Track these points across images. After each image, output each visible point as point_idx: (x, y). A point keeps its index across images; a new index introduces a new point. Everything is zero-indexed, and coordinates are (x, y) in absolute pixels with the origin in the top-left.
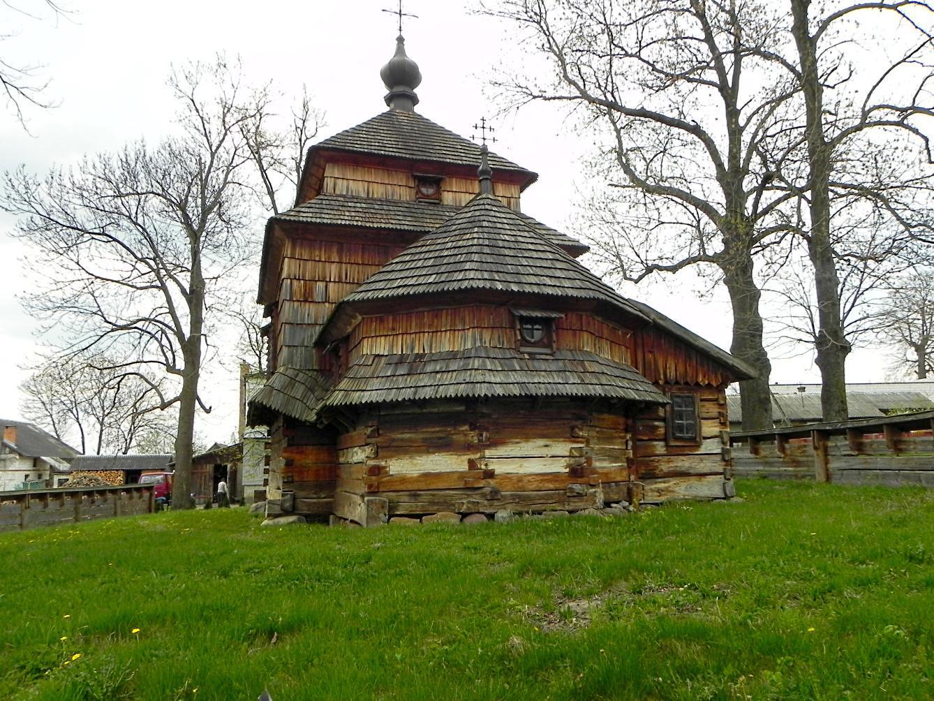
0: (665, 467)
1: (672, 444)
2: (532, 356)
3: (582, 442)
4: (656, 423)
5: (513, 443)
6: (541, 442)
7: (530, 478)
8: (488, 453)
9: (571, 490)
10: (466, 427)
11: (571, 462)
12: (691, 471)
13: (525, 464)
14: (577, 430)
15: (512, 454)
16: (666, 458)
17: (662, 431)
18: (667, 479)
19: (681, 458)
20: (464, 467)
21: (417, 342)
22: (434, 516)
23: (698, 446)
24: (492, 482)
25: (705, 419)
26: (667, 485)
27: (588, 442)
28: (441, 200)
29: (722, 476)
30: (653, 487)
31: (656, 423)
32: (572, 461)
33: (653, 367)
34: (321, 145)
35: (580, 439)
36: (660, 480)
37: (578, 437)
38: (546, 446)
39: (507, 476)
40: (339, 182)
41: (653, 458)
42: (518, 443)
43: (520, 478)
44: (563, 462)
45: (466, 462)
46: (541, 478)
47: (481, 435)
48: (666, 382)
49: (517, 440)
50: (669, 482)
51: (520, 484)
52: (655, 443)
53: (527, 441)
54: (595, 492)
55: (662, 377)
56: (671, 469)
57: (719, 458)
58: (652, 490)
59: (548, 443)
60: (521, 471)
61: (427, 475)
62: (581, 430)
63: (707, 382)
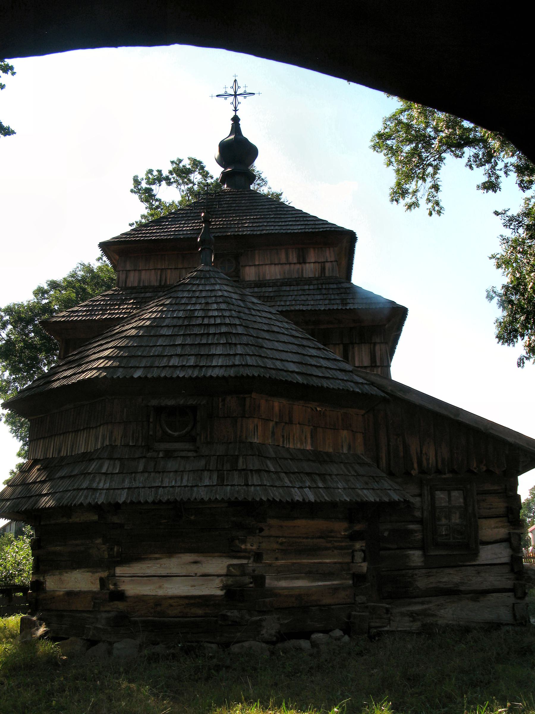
0: (422, 583)
1: (433, 553)
2: (169, 455)
3: (248, 558)
4: (412, 527)
5: (151, 559)
6: (188, 557)
7: (171, 601)
8: (119, 571)
9: (224, 617)
10: (99, 541)
11: (230, 582)
12: (462, 588)
13: (166, 585)
14: (237, 542)
15: (150, 572)
16: (424, 571)
17: (419, 536)
18: (427, 599)
19: (447, 570)
20: (96, 587)
21: (64, 444)
22: (67, 641)
23: (475, 554)
24: (121, 606)
25: (485, 518)
26: (425, 606)
27: (258, 557)
28: (239, 277)
29: (510, 594)
30: (404, 609)
31: (412, 527)
32: (230, 581)
33: (402, 454)
34: (114, 240)
35: (242, 554)
36: (417, 600)
37: (239, 552)
38: (196, 562)
39: (141, 599)
40: (132, 274)
41: (404, 572)
42: (157, 559)
43: (158, 601)
44: (217, 582)
45: (98, 582)
46: (187, 601)
47: (112, 549)
48: (422, 471)
49: (157, 556)
50: (429, 602)
51: (159, 609)
52: (411, 552)
53: (170, 557)
54: (261, 620)
55: (416, 466)
56: (431, 586)
57: (506, 569)
58: (403, 614)
59: (198, 559)
60: (161, 593)
61: (70, 594)
62: (244, 542)
63: (484, 468)
